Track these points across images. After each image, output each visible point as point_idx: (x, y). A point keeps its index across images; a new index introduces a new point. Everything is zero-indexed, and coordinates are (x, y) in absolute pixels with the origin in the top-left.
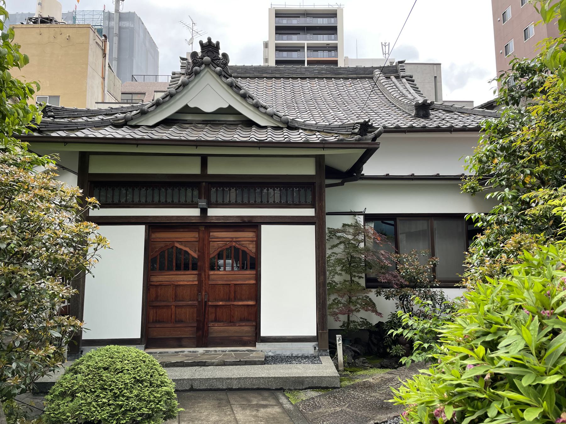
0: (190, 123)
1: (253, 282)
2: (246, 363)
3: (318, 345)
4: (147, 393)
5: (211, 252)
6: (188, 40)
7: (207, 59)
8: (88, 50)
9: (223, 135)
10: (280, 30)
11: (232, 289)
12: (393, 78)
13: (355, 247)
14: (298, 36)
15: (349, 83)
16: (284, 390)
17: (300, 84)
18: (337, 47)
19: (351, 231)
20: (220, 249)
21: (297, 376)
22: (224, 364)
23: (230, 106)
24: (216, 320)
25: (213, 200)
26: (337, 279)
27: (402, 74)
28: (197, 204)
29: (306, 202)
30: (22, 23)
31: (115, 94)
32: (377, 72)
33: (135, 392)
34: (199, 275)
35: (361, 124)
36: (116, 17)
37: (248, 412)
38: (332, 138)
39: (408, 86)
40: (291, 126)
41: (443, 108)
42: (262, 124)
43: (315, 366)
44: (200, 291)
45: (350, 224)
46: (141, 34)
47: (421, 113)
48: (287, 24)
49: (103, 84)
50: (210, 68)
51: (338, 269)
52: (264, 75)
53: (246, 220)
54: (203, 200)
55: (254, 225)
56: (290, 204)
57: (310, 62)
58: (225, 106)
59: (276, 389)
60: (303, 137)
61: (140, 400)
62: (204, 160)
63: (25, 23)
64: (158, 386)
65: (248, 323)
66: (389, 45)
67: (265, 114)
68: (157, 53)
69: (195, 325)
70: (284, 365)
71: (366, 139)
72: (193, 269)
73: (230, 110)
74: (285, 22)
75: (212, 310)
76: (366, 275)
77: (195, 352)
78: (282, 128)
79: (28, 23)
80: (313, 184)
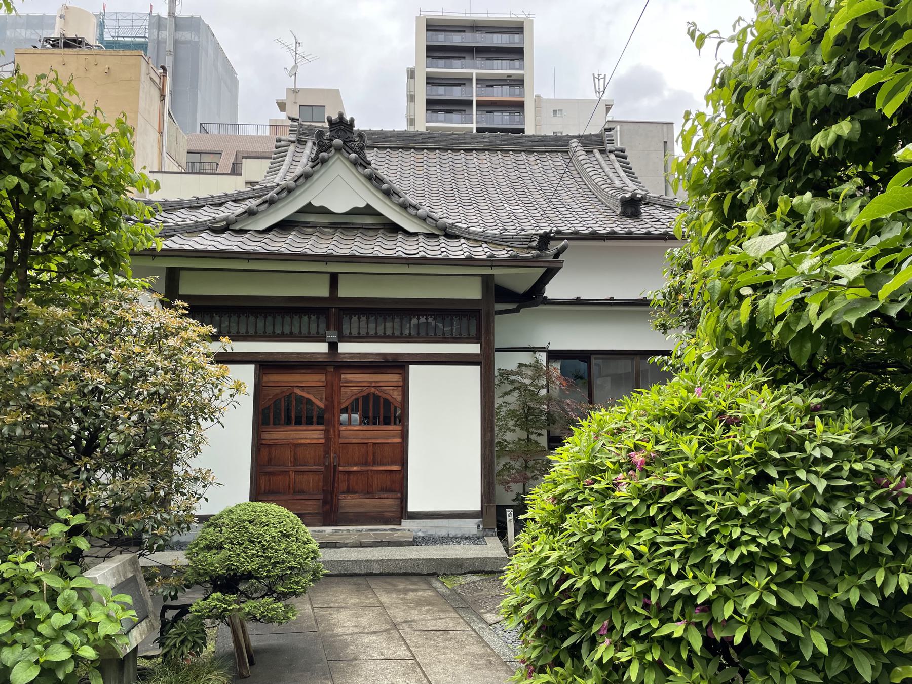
0: (314, 226)
1: (398, 440)
2: (389, 544)
3: (483, 523)
4: (295, 547)
5: (342, 401)
6: (289, 69)
7: (338, 142)
8: (138, 90)
9: (359, 246)
10: (433, 52)
11: (371, 449)
12: (596, 151)
13: (534, 395)
14: (462, 61)
15: (533, 159)
16: (438, 575)
17: (463, 160)
18: (523, 81)
19: (530, 373)
20: (354, 397)
21: (455, 557)
22: (361, 545)
23: (368, 206)
24: (349, 491)
25: (346, 332)
26: (509, 436)
27: (609, 147)
28: (325, 337)
29: (469, 335)
30: (35, 47)
31: (177, 157)
32: (574, 144)
33: (283, 546)
34: (326, 431)
35: (541, 236)
36: (170, 24)
37: (394, 596)
38: (503, 252)
39: (617, 165)
40: (450, 234)
41: (661, 202)
42: (412, 230)
43: (478, 547)
44: (327, 452)
45: (528, 363)
46: (211, 52)
47: (629, 211)
48: (446, 42)
49: (160, 142)
50: (342, 154)
51: (511, 423)
52: (412, 145)
53: (389, 358)
54: (332, 331)
55: (399, 365)
56: (448, 338)
57: (480, 104)
58: (362, 205)
59: (429, 574)
60: (466, 250)
61: (289, 553)
62: (334, 279)
63: (39, 45)
64: (305, 543)
65: (391, 495)
66: (605, 78)
67: (416, 216)
68: (234, 82)
69: (321, 496)
70: (439, 546)
71: (546, 256)
72: (318, 423)
73: (368, 211)
74: (441, 39)
75: (343, 477)
76: (548, 432)
77: (322, 531)
78: (438, 236)
79: (43, 47)
80: (479, 311)
